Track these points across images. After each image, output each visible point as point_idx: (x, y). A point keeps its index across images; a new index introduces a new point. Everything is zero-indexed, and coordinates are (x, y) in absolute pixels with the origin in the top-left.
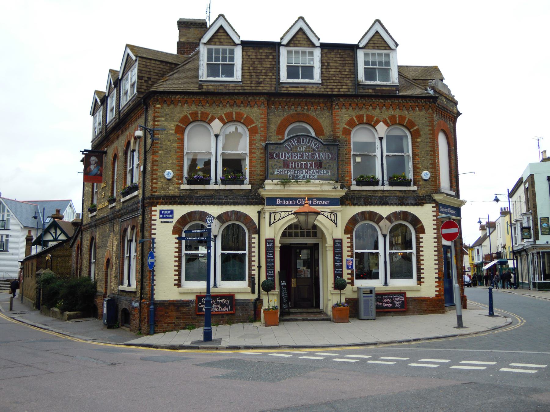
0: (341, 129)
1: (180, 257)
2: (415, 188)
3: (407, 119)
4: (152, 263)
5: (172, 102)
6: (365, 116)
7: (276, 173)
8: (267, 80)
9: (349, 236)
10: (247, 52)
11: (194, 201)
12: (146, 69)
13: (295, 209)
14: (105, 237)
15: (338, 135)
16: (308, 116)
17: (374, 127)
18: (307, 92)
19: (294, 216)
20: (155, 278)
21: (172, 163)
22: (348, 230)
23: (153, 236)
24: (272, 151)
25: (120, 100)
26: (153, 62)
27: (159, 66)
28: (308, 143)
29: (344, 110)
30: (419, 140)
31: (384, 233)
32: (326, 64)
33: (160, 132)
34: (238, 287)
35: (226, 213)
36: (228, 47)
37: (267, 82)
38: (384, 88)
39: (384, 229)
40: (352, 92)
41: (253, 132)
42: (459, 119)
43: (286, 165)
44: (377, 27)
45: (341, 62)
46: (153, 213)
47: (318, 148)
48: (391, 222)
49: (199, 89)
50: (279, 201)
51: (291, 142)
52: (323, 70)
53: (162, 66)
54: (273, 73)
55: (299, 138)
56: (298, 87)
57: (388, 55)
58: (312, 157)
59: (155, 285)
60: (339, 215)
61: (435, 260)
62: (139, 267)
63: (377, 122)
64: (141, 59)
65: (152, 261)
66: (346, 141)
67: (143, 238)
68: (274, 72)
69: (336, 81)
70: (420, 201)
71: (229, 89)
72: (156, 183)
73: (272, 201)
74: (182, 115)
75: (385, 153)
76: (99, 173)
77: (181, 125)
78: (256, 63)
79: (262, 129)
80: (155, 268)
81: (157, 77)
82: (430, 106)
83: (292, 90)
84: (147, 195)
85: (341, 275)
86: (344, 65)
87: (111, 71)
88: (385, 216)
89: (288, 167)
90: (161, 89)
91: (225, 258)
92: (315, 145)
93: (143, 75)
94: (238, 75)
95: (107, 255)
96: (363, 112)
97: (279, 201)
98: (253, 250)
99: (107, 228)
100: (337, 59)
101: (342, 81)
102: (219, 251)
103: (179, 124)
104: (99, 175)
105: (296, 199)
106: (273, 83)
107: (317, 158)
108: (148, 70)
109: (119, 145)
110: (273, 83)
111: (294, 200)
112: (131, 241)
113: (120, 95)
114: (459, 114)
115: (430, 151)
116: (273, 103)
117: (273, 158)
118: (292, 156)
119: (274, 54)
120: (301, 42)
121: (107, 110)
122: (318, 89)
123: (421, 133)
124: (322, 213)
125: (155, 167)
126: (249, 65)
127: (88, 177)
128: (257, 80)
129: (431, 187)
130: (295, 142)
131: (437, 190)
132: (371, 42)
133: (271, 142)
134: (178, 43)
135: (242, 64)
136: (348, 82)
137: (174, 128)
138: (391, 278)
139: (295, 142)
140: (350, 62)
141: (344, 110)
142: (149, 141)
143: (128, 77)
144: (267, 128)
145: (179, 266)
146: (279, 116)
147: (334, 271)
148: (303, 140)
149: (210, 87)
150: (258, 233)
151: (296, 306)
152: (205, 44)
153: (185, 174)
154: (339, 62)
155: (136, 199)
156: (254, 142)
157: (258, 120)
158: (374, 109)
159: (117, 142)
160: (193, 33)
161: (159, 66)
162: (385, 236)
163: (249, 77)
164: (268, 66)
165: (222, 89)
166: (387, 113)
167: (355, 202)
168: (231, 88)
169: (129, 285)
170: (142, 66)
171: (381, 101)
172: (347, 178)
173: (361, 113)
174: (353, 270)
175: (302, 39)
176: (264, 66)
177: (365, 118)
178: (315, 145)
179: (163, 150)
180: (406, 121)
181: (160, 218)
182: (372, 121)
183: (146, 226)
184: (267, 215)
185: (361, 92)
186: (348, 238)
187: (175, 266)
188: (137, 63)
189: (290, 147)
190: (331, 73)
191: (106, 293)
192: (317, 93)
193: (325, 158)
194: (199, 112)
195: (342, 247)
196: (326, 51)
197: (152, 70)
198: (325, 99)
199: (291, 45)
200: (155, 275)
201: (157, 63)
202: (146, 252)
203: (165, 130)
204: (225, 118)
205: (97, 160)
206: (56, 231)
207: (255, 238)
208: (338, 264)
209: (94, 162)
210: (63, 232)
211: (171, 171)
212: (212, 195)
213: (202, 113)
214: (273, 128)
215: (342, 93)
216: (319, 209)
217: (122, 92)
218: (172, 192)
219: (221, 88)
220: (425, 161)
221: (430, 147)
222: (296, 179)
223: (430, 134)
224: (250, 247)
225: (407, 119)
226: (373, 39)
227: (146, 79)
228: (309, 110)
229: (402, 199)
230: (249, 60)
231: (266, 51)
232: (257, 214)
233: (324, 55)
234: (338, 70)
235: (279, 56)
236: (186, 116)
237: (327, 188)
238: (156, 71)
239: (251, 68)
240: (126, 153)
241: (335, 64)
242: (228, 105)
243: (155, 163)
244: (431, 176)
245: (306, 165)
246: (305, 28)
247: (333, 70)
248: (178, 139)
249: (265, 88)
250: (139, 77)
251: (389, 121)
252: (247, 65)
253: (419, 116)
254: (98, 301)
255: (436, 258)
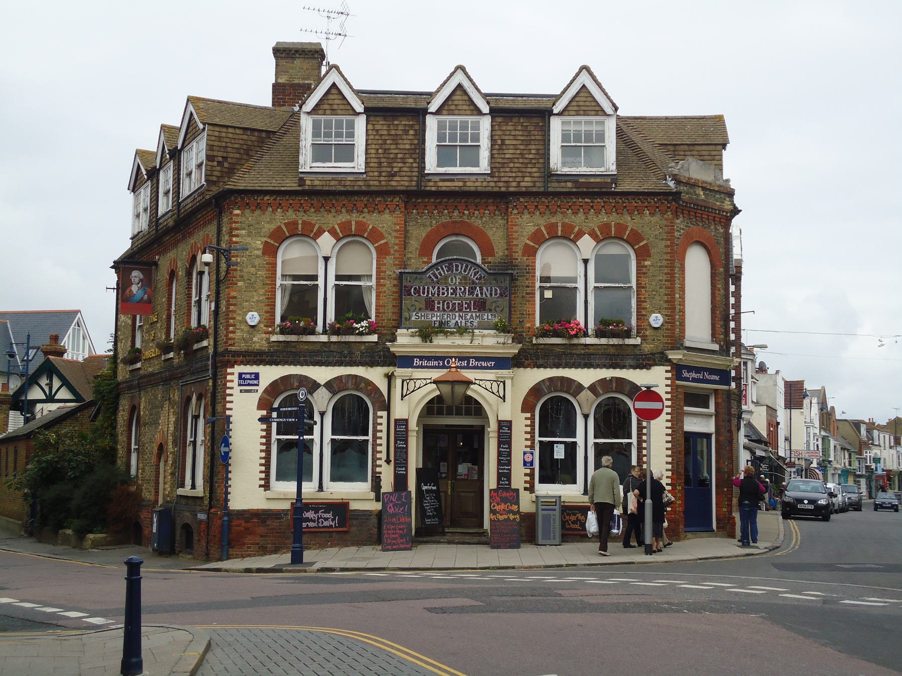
0: (521, 246)
1: (268, 444)
2: (638, 341)
3: (629, 229)
4: (227, 454)
5: (258, 206)
6: (560, 225)
7: (413, 318)
8: (405, 169)
9: (529, 415)
10: (374, 125)
11: (291, 359)
12: (220, 144)
13: (436, 374)
14: (155, 408)
15: (515, 255)
16: (469, 225)
17: (574, 241)
18: (467, 189)
19: (434, 386)
20: (230, 475)
21: (258, 301)
22: (527, 406)
23: (228, 413)
24: (409, 284)
25: (179, 184)
26: (231, 130)
27: (241, 137)
28: (465, 271)
29: (526, 216)
30: (646, 263)
31: (586, 411)
32: (499, 142)
33: (240, 253)
34: (356, 493)
35: (339, 379)
36: (471, 119)
37: (404, 174)
38: (592, 180)
39: (584, 405)
40: (539, 187)
41: (382, 252)
42: (736, 221)
43: (430, 305)
44: (585, 79)
45: (523, 138)
46: (229, 377)
47: (480, 279)
48: (597, 394)
49: (299, 186)
50: (417, 362)
51: (437, 269)
52: (495, 152)
53: (245, 137)
54: (415, 159)
55: (451, 264)
56: (453, 180)
57: (603, 123)
58: (471, 293)
59: (230, 486)
60: (508, 383)
61: (667, 456)
62: (209, 458)
63: (580, 235)
64: (211, 128)
65: (226, 449)
66: (528, 266)
67: (214, 414)
68: (417, 156)
69: (514, 170)
70: (644, 362)
71: (345, 186)
72: (234, 332)
73: (406, 361)
74: (273, 227)
75: (592, 284)
76: (146, 297)
77: (272, 242)
78: (388, 142)
79: (396, 248)
80: (230, 461)
81: (238, 156)
82: (669, 208)
83: (445, 186)
84: (221, 349)
85: (508, 476)
86: (527, 143)
87: (164, 128)
88: (586, 385)
89: (432, 309)
90: (241, 186)
91: (338, 448)
92: (475, 274)
93: (215, 153)
94: (359, 164)
95: (158, 438)
96: (557, 219)
97: (417, 362)
98: (379, 434)
99: (159, 392)
100: (517, 133)
101: (524, 170)
102: (328, 436)
103: (269, 240)
104: (145, 302)
105: (442, 358)
106: (414, 174)
107: (477, 295)
108: (224, 144)
109: (178, 255)
110: (414, 174)
111: (440, 360)
112: (196, 418)
113: (179, 174)
114: (736, 211)
115: (666, 281)
116: (415, 206)
117: (410, 294)
118: (439, 292)
119: (417, 127)
120: (460, 107)
121: (158, 192)
122: (485, 184)
123: (652, 251)
124: (477, 382)
125: (232, 308)
126: (377, 147)
127: (124, 300)
128: (389, 169)
129: (665, 340)
130: (444, 271)
131: (677, 343)
132: (574, 104)
133: (407, 271)
134: (274, 86)
135: (367, 145)
136: (534, 170)
137: (261, 247)
138: (540, 482)
139: (444, 271)
140: (538, 137)
141: (526, 216)
142: (223, 266)
143: (191, 148)
144: (405, 245)
145: (268, 458)
146: (424, 226)
147: (498, 469)
148: (457, 266)
149: (317, 183)
150: (387, 408)
151: (454, 524)
152: (308, 113)
153: (278, 320)
154: (520, 138)
155: (204, 353)
156: (383, 268)
157: (390, 234)
158: (575, 213)
159: (175, 251)
160: (299, 69)
161: (241, 137)
162: (586, 417)
163: (376, 165)
164: (408, 147)
165: (334, 186)
166: (596, 220)
167: (541, 362)
168: (348, 183)
169: (193, 487)
170: (213, 138)
171: (587, 200)
172: (528, 325)
173: (553, 220)
174: (533, 469)
175: (461, 103)
176: (401, 146)
177: (560, 228)
178: (475, 274)
179: (244, 281)
180: (628, 232)
181: (240, 385)
182: (571, 234)
183: (219, 396)
184: (398, 382)
185: (554, 187)
186: (526, 419)
187: (261, 458)
188: (205, 133)
189: (437, 277)
190: (507, 156)
191: (157, 501)
192: (483, 189)
193: (491, 294)
194: (300, 222)
195: (511, 433)
196: (499, 120)
197: (229, 145)
198: (495, 198)
199: (444, 112)
200: (230, 472)
201: (238, 131)
202: (218, 437)
203: (247, 249)
204: (338, 231)
205: (142, 276)
206: (51, 381)
207: (381, 417)
208: (504, 459)
209: (137, 280)
210: (65, 383)
211: (255, 314)
212: (318, 351)
213: (304, 223)
214: (414, 245)
215: (524, 189)
216: (470, 375)
217: (183, 172)
218: (257, 346)
219: (333, 183)
220: (657, 297)
221: (666, 274)
222: (442, 329)
223: (666, 253)
224: (375, 431)
225: (629, 229)
226: (577, 99)
227: (220, 159)
228: (471, 215)
229: (614, 359)
230: (377, 137)
231: (403, 123)
232: (386, 381)
233: (497, 128)
234: (518, 152)
235: (424, 131)
236: (280, 227)
237: (490, 341)
238: (236, 146)
239: (380, 151)
240: (189, 274)
241: (514, 142)
242: (343, 210)
243: (232, 301)
244: (665, 322)
245: (460, 305)
246: (467, 85)
247: (511, 151)
248: (267, 264)
249: (402, 182)
250: (209, 158)
251: (599, 233)
252: (373, 146)
253: (650, 224)
254: (144, 515)
255: (669, 452)
